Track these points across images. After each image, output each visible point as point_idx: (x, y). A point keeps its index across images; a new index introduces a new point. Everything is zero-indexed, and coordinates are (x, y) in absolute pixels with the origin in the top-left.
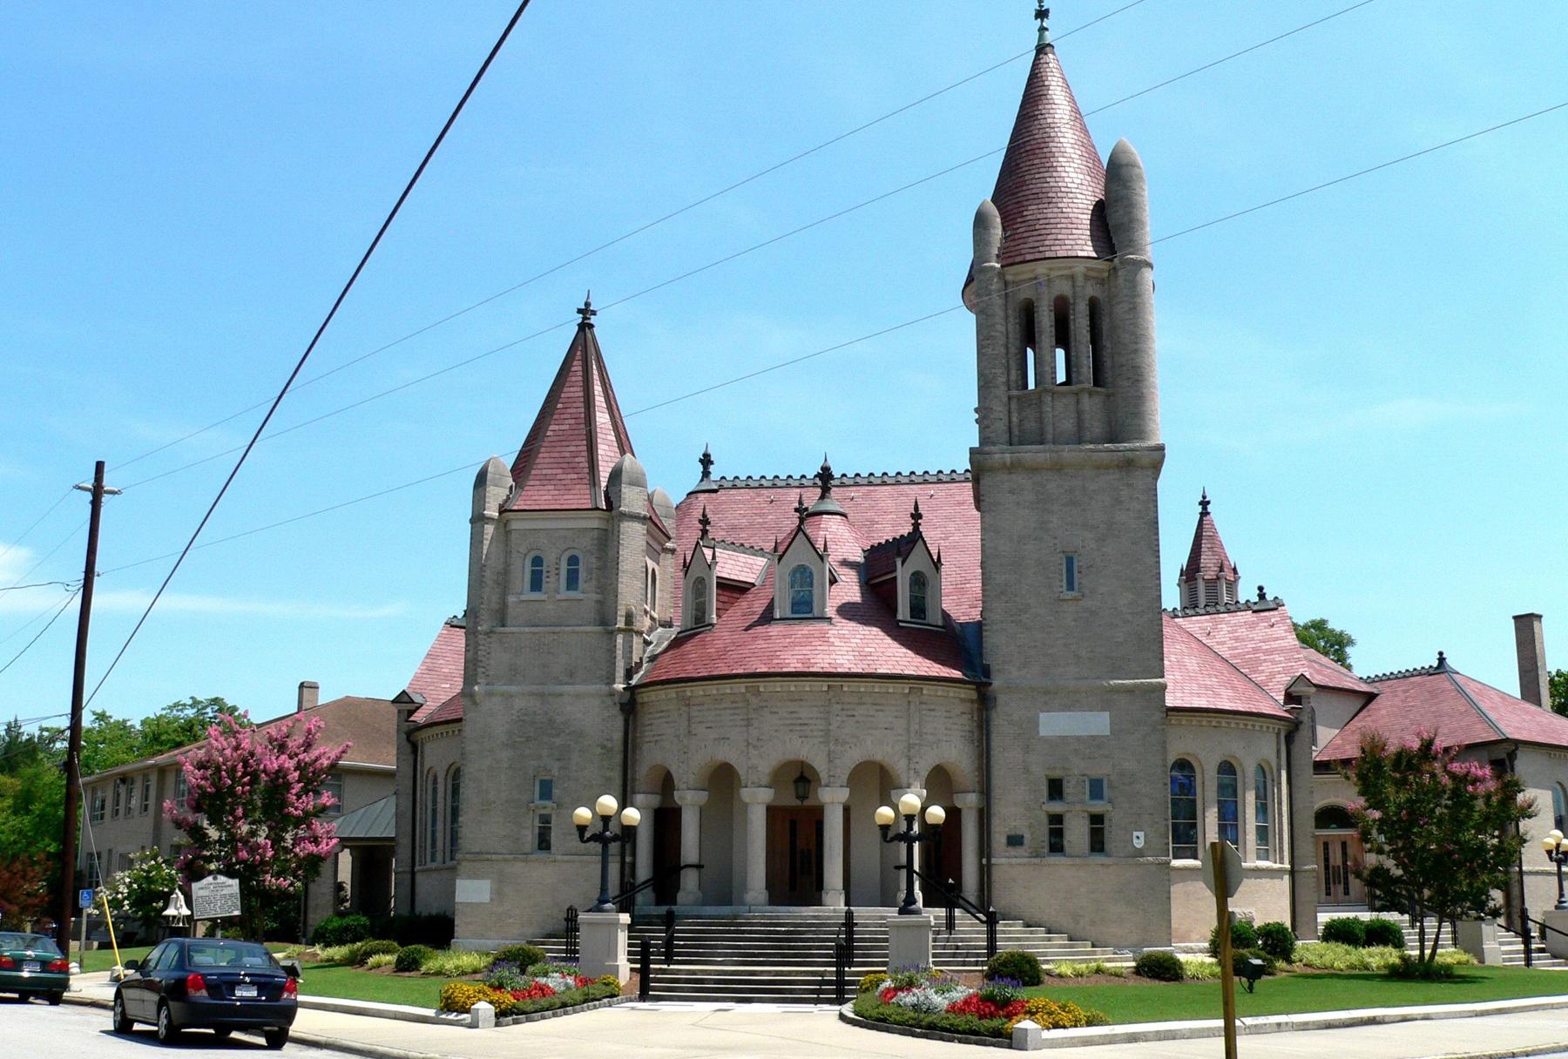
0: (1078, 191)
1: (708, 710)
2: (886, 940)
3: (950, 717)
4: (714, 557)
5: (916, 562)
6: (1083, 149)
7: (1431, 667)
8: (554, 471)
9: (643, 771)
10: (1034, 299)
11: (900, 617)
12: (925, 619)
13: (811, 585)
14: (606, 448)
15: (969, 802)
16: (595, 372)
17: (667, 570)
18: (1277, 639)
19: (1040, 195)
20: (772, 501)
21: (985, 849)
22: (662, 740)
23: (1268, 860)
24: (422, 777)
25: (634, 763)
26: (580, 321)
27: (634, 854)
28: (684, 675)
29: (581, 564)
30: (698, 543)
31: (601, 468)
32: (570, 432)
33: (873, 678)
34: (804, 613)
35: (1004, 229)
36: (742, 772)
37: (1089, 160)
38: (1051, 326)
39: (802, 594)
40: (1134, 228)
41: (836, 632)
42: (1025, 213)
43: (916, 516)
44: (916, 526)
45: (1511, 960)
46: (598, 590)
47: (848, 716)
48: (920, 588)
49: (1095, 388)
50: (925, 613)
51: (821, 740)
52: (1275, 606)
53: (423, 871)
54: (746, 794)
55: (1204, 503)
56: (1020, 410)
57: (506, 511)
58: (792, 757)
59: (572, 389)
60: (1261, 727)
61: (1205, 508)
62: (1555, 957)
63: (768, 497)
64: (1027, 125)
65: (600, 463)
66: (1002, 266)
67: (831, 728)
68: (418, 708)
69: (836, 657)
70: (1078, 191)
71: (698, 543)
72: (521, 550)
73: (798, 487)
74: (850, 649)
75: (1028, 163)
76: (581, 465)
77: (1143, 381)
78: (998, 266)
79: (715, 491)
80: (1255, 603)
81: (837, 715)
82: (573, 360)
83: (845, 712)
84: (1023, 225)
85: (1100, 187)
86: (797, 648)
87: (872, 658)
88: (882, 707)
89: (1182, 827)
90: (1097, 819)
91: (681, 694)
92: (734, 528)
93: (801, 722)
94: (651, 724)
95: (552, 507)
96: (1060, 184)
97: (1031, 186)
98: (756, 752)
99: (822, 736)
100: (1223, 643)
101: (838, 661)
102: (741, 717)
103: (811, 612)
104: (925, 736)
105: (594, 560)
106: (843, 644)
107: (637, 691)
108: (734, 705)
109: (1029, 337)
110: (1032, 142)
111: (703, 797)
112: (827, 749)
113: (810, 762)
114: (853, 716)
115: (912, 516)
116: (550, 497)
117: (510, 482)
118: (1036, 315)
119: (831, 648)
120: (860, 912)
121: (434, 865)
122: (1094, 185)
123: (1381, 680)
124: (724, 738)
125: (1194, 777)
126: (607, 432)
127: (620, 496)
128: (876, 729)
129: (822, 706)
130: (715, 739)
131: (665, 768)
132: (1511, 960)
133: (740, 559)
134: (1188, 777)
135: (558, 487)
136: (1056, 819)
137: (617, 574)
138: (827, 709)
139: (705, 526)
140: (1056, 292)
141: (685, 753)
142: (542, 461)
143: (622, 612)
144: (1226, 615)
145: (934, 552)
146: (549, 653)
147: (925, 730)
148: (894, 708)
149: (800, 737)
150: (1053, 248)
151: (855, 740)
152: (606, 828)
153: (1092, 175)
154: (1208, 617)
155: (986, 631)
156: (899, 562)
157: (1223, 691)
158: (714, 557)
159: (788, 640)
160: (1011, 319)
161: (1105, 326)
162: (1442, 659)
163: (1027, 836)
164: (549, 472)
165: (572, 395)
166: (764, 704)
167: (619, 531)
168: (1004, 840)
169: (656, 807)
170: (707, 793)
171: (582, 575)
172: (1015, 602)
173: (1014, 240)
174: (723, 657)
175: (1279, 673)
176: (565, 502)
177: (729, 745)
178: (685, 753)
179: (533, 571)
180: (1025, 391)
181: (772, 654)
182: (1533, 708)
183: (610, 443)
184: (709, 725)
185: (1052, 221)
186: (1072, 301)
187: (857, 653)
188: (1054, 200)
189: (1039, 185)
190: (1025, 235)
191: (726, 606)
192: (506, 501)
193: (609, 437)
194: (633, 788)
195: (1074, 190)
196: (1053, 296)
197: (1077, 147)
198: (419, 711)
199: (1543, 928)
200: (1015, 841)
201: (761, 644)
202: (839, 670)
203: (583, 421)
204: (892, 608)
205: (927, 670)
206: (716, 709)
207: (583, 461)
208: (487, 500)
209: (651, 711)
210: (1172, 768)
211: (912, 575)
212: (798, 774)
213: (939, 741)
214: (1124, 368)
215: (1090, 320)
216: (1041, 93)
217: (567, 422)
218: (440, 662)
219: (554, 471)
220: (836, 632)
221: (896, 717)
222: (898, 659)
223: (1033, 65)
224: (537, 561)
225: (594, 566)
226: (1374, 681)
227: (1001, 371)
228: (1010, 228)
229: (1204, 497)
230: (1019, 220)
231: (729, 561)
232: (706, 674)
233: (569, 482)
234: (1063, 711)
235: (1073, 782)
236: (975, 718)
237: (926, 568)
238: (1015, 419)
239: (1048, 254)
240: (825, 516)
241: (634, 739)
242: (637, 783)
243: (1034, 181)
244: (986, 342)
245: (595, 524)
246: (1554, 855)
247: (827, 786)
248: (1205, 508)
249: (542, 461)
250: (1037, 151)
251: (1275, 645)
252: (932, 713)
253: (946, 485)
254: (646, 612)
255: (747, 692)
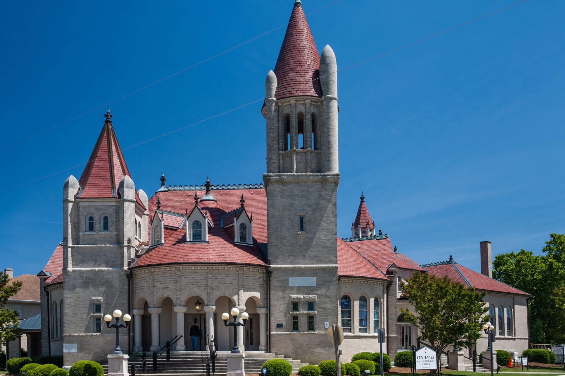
0: (308, 67)
1: (161, 277)
2: (227, 363)
3: (255, 279)
4: (162, 217)
5: (242, 219)
6: (312, 49)
7: (447, 261)
8: (97, 182)
9: (136, 301)
10: (289, 113)
11: (236, 240)
12: (246, 241)
13: (201, 228)
14: (118, 173)
15: (262, 312)
16: (112, 141)
17: (144, 221)
18: (385, 250)
19: (293, 69)
20: (189, 196)
21: (268, 329)
22: (143, 289)
23: (366, 332)
24: (51, 304)
25: (133, 298)
26: (106, 120)
27: (134, 333)
28: (151, 264)
29: (109, 220)
30: (156, 211)
31: (116, 181)
32: (103, 166)
33: (224, 264)
34: (198, 239)
35: (278, 83)
36: (174, 300)
37: (314, 54)
38: (296, 125)
39: (197, 231)
40: (330, 84)
41: (210, 246)
42: (287, 77)
43: (242, 201)
44: (242, 205)
45: (468, 369)
46: (116, 230)
47: (215, 279)
48: (244, 229)
49: (315, 151)
50: (246, 239)
51: (205, 288)
52: (385, 238)
53: (53, 341)
54: (176, 309)
55: (362, 198)
56: (283, 159)
57: (77, 198)
58: (193, 295)
59: (103, 148)
60: (377, 283)
61: (362, 200)
62: (485, 368)
63: (188, 194)
64: (289, 38)
65: (115, 179)
66: (277, 99)
67: (208, 283)
68: (48, 278)
69: (210, 256)
70: (308, 67)
71: (156, 211)
72: (84, 214)
73: (199, 190)
74: (216, 253)
75: (289, 55)
76: (108, 180)
77: (332, 147)
78: (275, 99)
79: (167, 191)
80: (378, 236)
81: (211, 279)
82: (103, 136)
83: (214, 277)
84: (286, 82)
85: (318, 66)
86: (195, 253)
87: (224, 256)
88: (228, 276)
89: (345, 321)
90: (311, 317)
91: (150, 271)
92: (174, 206)
93: (197, 281)
94: (139, 283)
95: (96, 197)
96: (302, 64)
97: (290, 65)
98: (179, 293)
99: (205, 287)
100: (365, 252)
101: (211, 258)
102: (173, 279)
103: (201, 238)
104: (245, 286)
105: (114, 218)
106: (213, 251)
107: (133, 270)
108: (170, 275)
109: (287, 129)
110: (291, 46)
111: (159, 310)
112: (207, 291)
113: (201, 297)
114: (217, 279)
115: (241, 201)
116: (95, 193)
117: (78, 186)
118: (290, 120)
119: (208, 253)
120: (220, 353)
121: (57, 339)
122: (315, 65)
123: (428, 266)
124: (167, 288)
125: (351, 302)
126: (118, 166)
127: (124, 192)
128: (226, 283)
129: (204, 275)
130: (163, 288)
131: (145, 300)
132: (468, 369)
133: (173, 218)
134: (348, 302)
135: (98, 189)
136: (295, 317)
137: (124, 224)
138: (207, 276)
139: (159, 205)
140: (298, 111)
141: (152, 293)
142: (91, 178)
143: (126, 239)
144: (366, 241)
145: (250, 216)
146: (97, 255)
147: (245, 284)
148: (233, 276)
149: (196, 287)
150: (297, 92)
151: (217, 288)
152: (117, 322)
153: (315, 61)
154: (359, 242)
155: (269, 246)
156: (235, 219)
157: (362, 269)
158: (162, 217)
159: (191, 250)
160: (280, 122)
161: (318, 124)
162: (451, 259)
163: (284, 324)
164: (95, 182)
165: (103, 151)
166: (182, 274)
167: (124, 207)
168: (275, 325)
169: (142, 314)
170: (161, 309)
171: (110, 224)
172: (280, 235)
173: (282, 88)
174: (166, 256)
175: (385, 263)
176: (101, 195)
177: (169, 290)
178: (152, 293)
179: (104, 222)
180: (286, 151)
181: (185, 255)
182: (485, 277)
183: (119, 171)
184: (161, 282)
185: (297, 80)
186: (305, 114)
187: (218, 255)
188: (299, 71)
189: (293, 65)
190: (287, 86)
191: (168, 236)
192: (77, 194)
193: (119, 168)
194: (133, 307)
195: (307, 67)
196: (297, 112)
197: (309, 48)
198: (49, 279)
199: (481, 357)
200: (280, 326)
201: (181, 251)
202: (211, 261)
203: (108, 162)
204: (233, 239)
205: (246, 261)
206: (164, 276)
207: (109, 177)
208: (69, 194)
209: (139, 277)
210: (342, 299)
211: (241, 224)
212: (197, 301)
213: (250, 288)
214: (325, 142)
215: (312, 122)
216: (295, 24)
217: (101, 162)
218: (57, 259)
219: (97, 182)
220: (210, 246)
221: (234, 279)
222: (234, 257)
223: (293, 12)
224: (91, 219)
225: (114, 220)
226: (425, 267)
227: (276, 143)
228: (280, 83)
229: (362, 195)
230: (284, 80)
231: (169, 219)
232: (159, 263)
233: (103, 186)
234: (298, 277)
235: (302, 304)
236: (265, 280)
237: (246, 222)
238: (281, 163)
239: (295, 94)
240: (207, 201)
241: (133, 288)
242: (134, 305)
243: (291, 63)
244: (270, 131)
245: (114, 204)
246: (487, 331)
247: (207, 305)
248: (362, 200)
249: (91, 178)
250: (293, 50)
251: (384, 252)
252: (248, 278)
253: (258, 190)
254: (136, 239)
255: (175, 270)
